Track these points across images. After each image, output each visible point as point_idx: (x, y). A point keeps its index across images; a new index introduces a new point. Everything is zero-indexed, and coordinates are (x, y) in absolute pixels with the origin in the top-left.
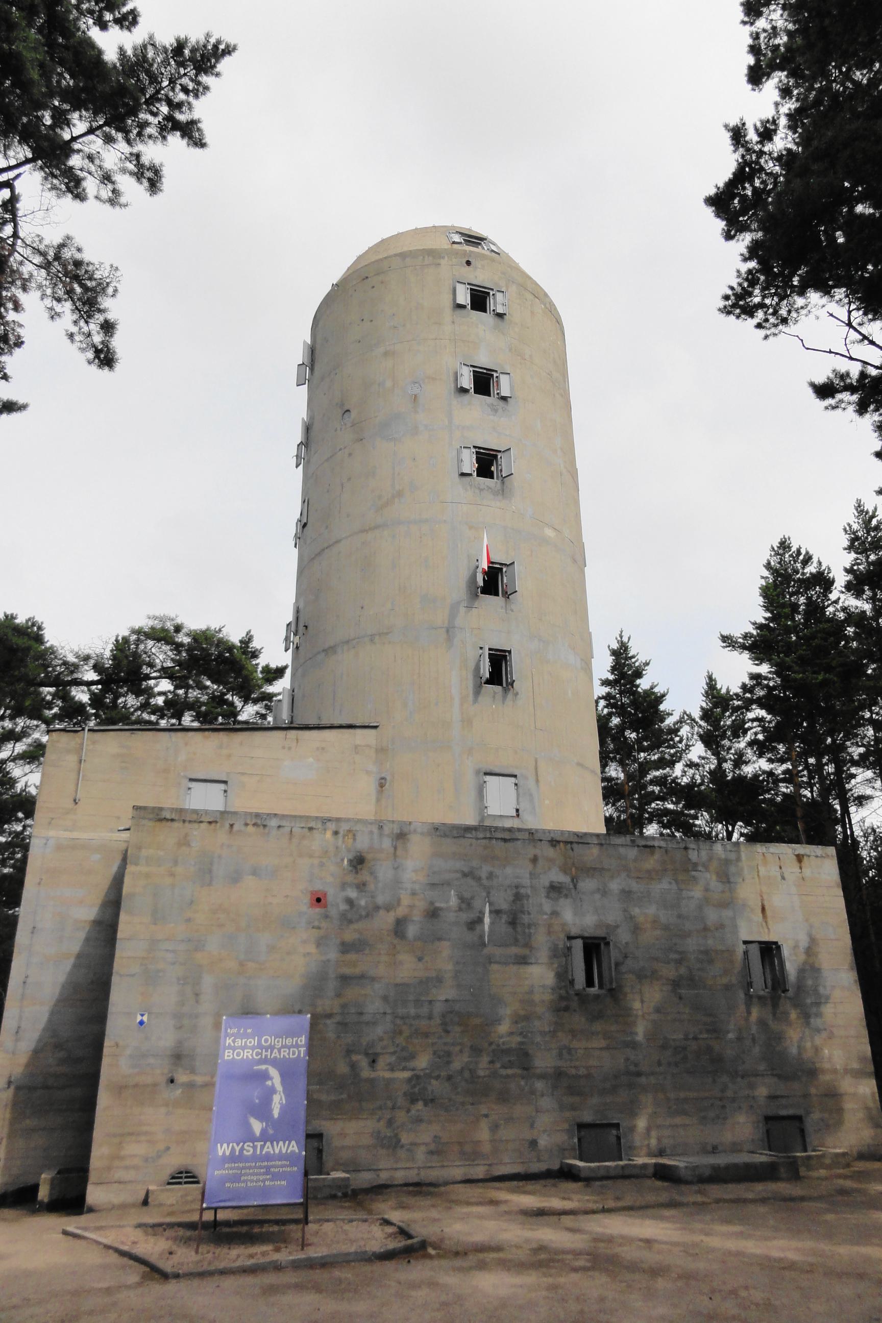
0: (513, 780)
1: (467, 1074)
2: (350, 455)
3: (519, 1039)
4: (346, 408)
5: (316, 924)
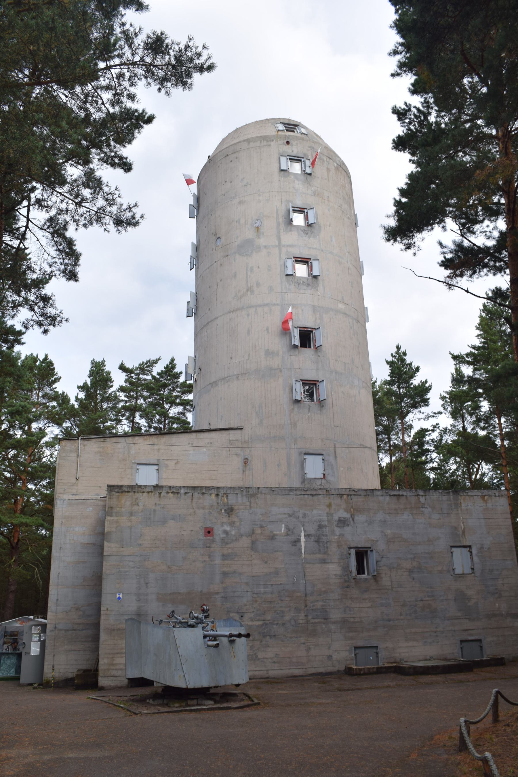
0: (321, 457)
1: (293, 622)
2: (221, 265)
3: (322, 603)
4: (218, 236)
5: (208, 545)
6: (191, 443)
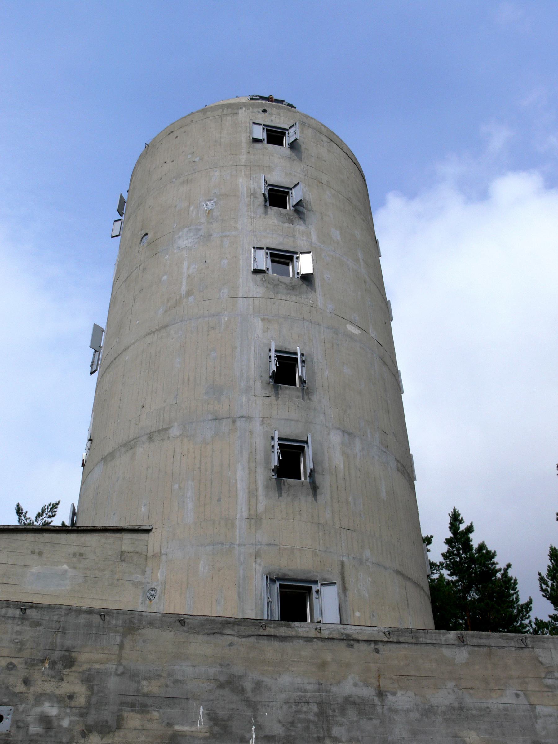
6: (37, 551)
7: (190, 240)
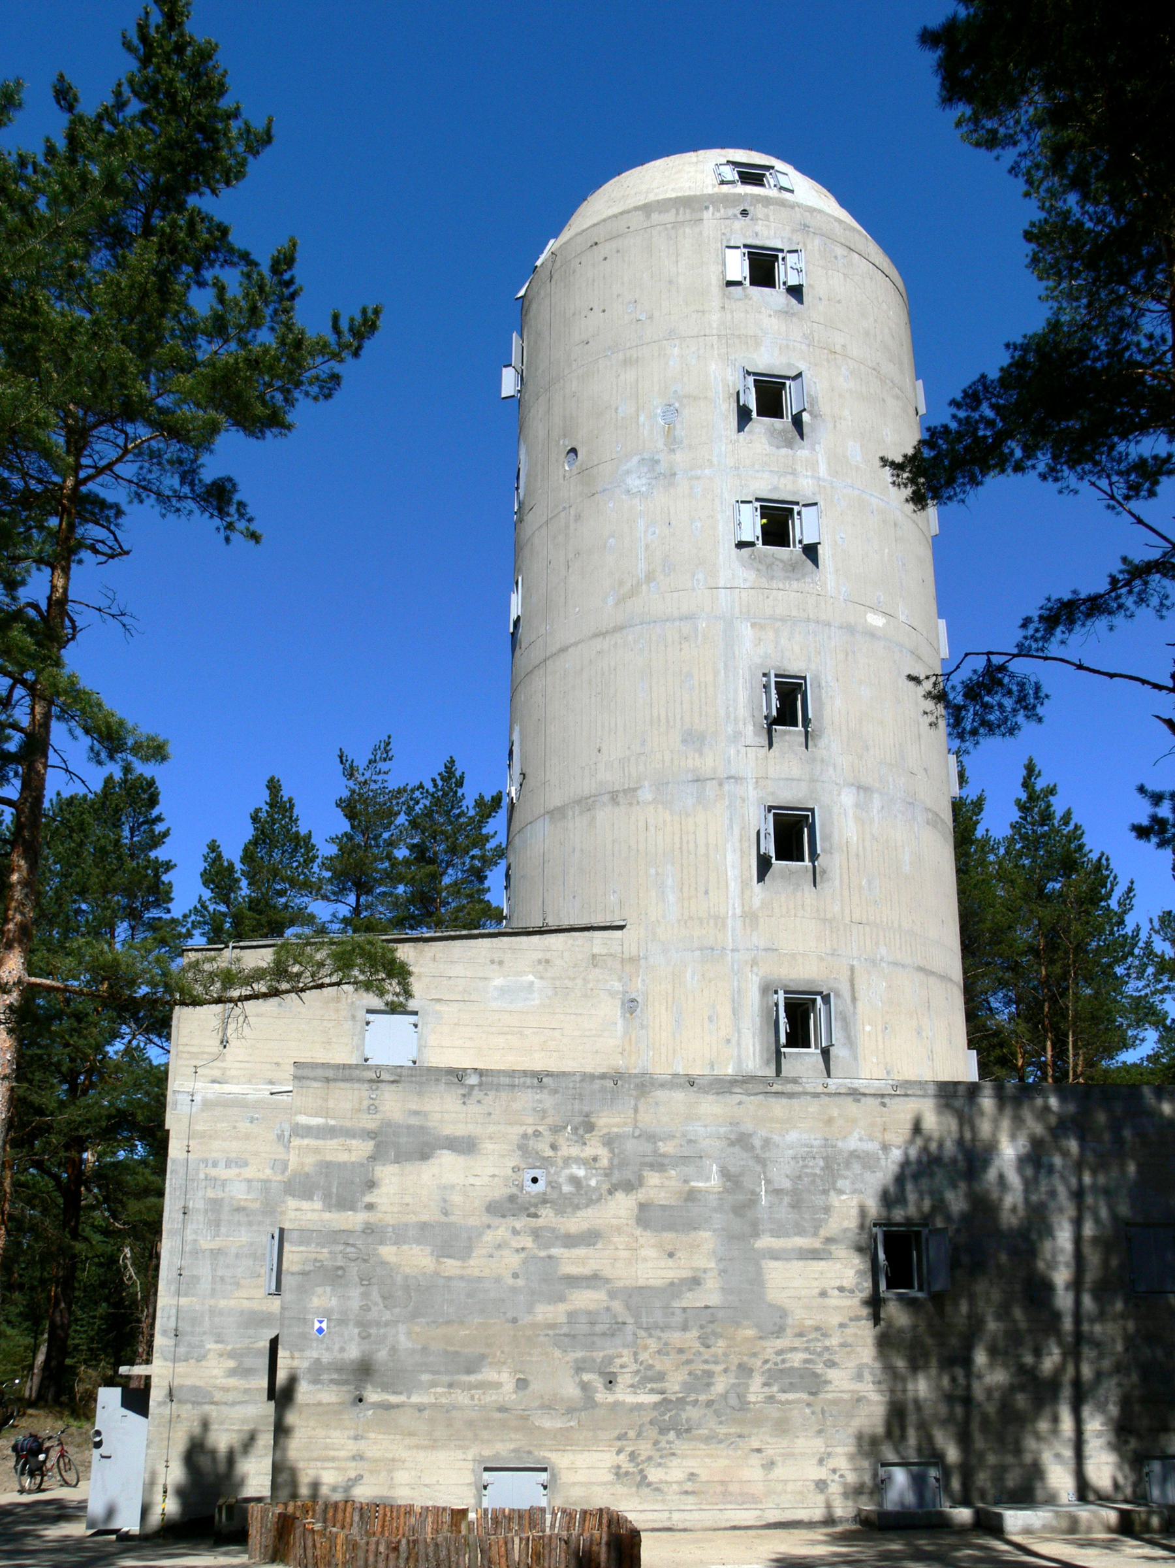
3: (807, 1356)
5: (532, 1210)
7: (644, 481)
